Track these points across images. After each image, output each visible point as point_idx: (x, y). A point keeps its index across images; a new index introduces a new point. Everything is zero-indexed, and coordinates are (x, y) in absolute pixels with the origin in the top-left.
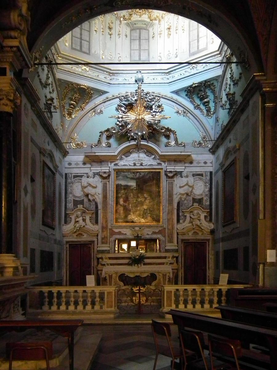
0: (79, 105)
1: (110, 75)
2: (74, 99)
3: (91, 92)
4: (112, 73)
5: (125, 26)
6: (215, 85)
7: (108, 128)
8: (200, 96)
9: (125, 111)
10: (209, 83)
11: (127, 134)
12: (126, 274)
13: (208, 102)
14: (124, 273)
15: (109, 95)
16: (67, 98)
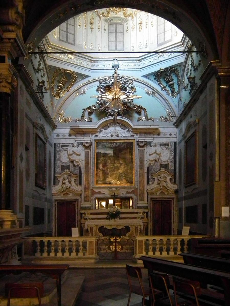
0: (65, 87)
1: (91, 62)
2: (62, 82)
3: (75, 76)
4: (93, 61)
5: (104, 21)
6: (178, 71)
7: (90, 106)
8: (166, 80)
9: (104, 92)
10: (173, 69)
11: (105, 111)
12: (105, 226)
13: (173, 84)
14: (103, 226)
15: (91, 79)
16: (55, 81)
